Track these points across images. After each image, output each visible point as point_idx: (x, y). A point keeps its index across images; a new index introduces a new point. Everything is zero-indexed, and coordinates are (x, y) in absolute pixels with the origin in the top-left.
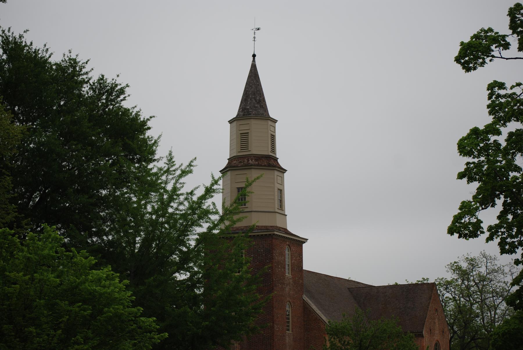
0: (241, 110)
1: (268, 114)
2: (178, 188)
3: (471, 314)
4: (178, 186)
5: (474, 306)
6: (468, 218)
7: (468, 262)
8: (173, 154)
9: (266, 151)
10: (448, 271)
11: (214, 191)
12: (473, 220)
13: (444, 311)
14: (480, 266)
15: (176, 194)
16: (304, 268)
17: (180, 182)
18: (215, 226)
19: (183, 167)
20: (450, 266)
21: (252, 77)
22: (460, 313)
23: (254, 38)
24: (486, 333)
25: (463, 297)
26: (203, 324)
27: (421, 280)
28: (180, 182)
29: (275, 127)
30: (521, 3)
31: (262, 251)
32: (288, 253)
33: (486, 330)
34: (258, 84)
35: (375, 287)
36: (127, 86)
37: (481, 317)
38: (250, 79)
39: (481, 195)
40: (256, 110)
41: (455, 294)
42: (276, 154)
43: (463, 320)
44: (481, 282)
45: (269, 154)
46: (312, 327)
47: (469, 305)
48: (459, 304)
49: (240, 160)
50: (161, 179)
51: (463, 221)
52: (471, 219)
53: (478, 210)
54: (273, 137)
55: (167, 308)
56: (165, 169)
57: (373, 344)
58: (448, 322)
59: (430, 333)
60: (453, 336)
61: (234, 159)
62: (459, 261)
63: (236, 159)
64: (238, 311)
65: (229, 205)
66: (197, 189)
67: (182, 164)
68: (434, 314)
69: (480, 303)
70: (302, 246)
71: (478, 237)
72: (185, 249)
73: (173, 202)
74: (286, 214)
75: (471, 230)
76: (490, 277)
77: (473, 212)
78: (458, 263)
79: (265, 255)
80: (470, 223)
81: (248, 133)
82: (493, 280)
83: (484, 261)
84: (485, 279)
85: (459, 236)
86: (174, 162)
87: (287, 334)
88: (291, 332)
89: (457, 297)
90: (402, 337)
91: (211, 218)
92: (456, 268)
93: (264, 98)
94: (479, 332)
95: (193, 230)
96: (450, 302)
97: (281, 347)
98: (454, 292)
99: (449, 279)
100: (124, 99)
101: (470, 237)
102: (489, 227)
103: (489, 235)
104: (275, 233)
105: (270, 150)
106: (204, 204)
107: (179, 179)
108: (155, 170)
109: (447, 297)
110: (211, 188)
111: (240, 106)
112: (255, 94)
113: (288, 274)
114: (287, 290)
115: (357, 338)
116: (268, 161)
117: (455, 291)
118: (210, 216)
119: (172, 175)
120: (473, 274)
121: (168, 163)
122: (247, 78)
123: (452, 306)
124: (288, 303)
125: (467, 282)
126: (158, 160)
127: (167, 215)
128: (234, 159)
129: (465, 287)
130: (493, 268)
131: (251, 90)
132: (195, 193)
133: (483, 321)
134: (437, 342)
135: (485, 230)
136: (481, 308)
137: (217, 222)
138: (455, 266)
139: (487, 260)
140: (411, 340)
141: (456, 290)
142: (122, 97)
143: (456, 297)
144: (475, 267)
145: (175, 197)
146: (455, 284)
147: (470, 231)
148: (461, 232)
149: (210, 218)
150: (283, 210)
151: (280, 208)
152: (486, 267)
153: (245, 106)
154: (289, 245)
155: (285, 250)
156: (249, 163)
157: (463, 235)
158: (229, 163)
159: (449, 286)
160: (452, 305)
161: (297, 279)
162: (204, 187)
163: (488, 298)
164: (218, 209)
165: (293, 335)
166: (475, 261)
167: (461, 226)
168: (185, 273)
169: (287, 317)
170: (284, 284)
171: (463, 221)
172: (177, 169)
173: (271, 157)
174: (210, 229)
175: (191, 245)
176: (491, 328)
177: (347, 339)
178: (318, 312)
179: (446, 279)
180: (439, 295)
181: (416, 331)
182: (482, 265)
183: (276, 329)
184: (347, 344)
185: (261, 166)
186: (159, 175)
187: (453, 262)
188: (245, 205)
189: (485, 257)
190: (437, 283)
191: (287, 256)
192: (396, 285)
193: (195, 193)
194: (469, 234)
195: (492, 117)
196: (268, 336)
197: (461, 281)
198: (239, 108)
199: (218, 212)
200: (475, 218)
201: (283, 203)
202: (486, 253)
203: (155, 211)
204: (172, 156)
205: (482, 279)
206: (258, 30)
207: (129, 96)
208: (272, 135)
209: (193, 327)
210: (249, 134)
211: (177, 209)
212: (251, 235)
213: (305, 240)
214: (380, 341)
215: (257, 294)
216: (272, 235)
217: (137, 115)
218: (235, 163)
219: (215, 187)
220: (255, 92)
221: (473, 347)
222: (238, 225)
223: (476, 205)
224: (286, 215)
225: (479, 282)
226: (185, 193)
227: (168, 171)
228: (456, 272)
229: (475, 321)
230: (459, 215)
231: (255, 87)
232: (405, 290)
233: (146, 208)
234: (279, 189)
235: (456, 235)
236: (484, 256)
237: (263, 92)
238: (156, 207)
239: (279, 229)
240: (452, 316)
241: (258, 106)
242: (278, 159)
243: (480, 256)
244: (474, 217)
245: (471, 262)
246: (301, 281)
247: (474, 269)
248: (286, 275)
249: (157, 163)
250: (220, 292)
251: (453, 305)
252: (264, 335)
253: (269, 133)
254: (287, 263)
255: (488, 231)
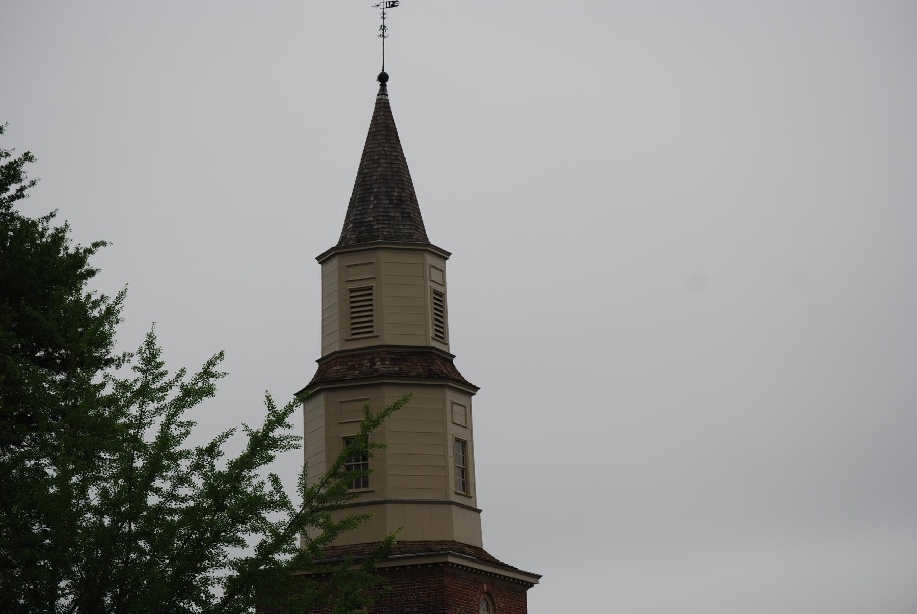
0: (351, 226)
1: (426, 235)
4: (175, 431)
8: (158, 344)
9: (424, 339)
11: (275, 444)
17: (179, 420)
18: (280, 540)
19: (187, 380)
21: (379, 137)
23: (383, 28)
28: (179, 420)
29: (443, 272)
34: (394, 154)
36: (28, 157)
38: (373, 142)
40: (391, 226)
42: (447, 344)
45: (429, 345)
49: (350, 363)
50: (126, 415)
54: (440, 299)
56: (137, 386)
61: (333, 360)
63: (339, 360)
65: (318, 483)
66: (225, 439)
67: (182, 370)
70: (526, 592)
74: (479, 507)
81: (371, 288)
86: (161, 364)
93: (412, 194)
100: (20, 194)
104: (451, 559)
105: (431, 333)
106: (249, 480)
107: (175, 413)
108: (108, 391)
110: (266, 435)
111: (348, 216)
112: (389, 182)
116: (426, 364)
118: (265, 514)
119: (156, 401)
121: (145, 368)
122: (365, 140)
126: (118, 362)
128: (335, 361)
131: (377, 171)
132: (220, 449)
137: (286, 530)
142: (13, 189)
145: (165, 463)
150: (471, 497)
153: (361, 214)
154: (488, 593)
156: (376, 371)
158: (319, 371)
162: (247, 432)
172: (169, 385)
173: (435, 354)
174: (265, 551)
175: (213, 596)
185: (408, 376)
186: (122, 403)
188: (366, 484)
193: (220, 449)
198: (346, 221)
199: (288, 502)
201: (471, 476)
203: (109, 505)
204: (155, 347)
206: (393, 6)
207: (33, 183)
208: (435, 292)
210: (374, 291)
211: (171, 496)
212: (383, 569)
213: (532, 579)
216: (441, 565)
217: (58, 238)
218: (338, 371)
219: (278, 432)
220: (387, 175)
222: (342, 540)
224: (480, 511)
226: (193, 450)
227: (144, 393)
231: (387, 163)
233: (83, 494)
237: (409, 176)
238: (112, 493)
239: (462, 549)
241: (398, 214)
242: (455, 356)
249: (116, 371)
253: (429, 288)
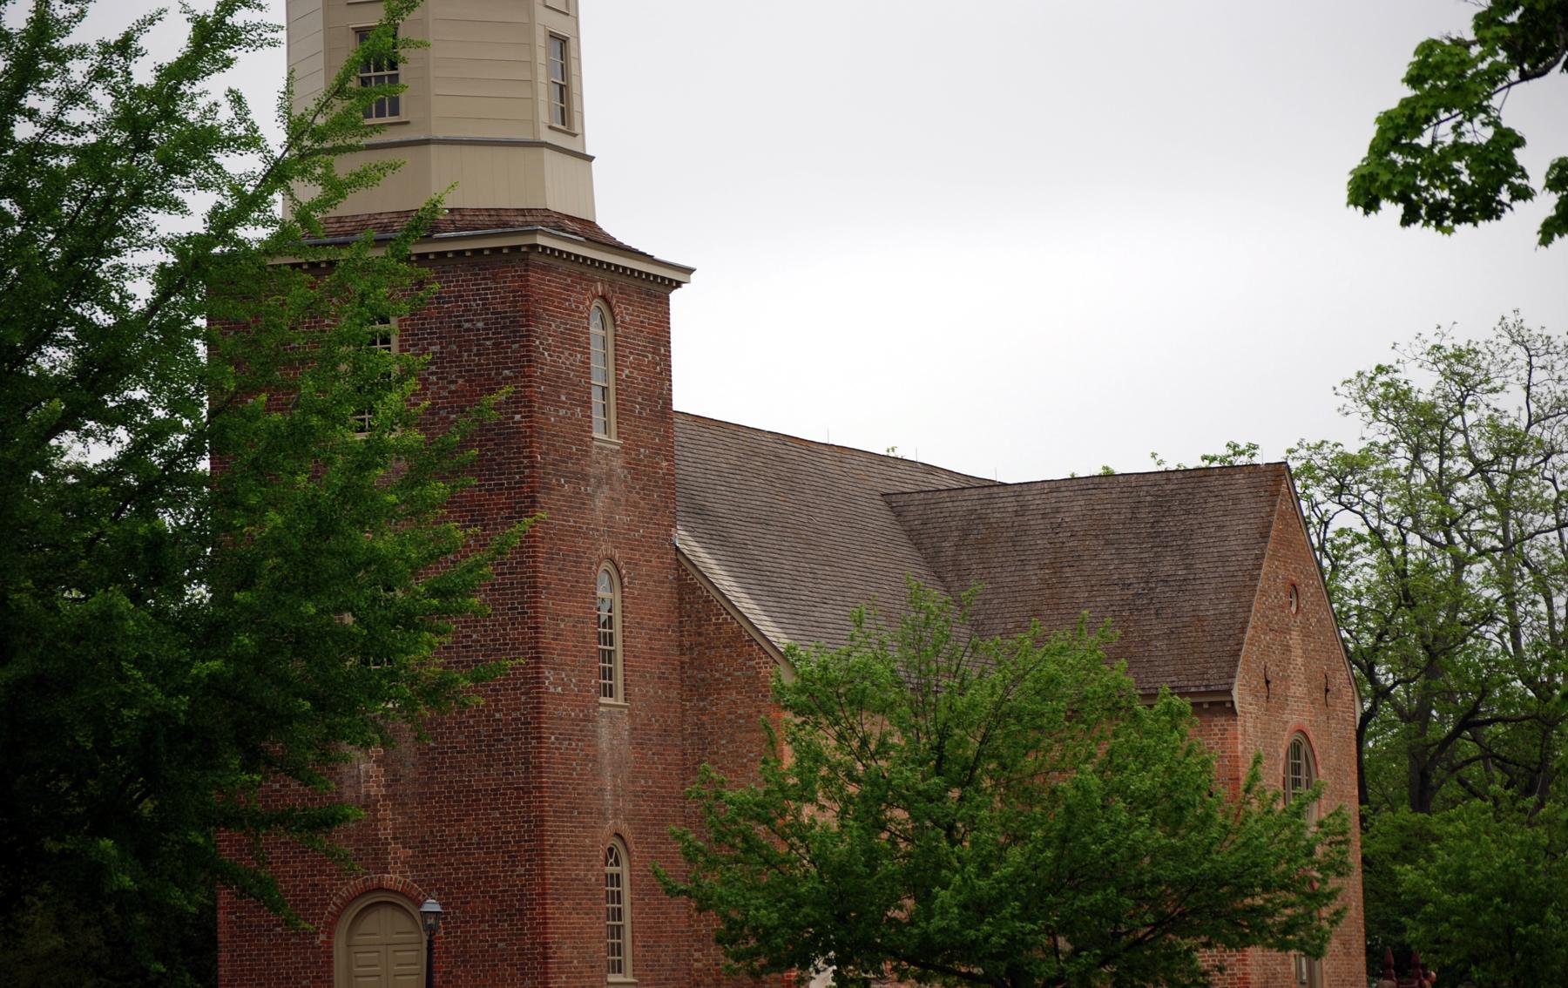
2: (58, 20)
3: (1455, 608)
5: (1471, 572)
6: (1452, 122)
7: (1442, 366)
10: (1346, 409)
12: (1478, 133)
13: (1330, 594)
14: (1498, 383)
15: (50, 49)
16: (679, 404)
18: (248, 204)
20: (1354, 389)
22: (1403, 602)
24: (1530, 693)
25: (1415, 528)
26: (194, 671)
27: (1222, 451)
30: (1424, 39)
31: (480, 325)
32: (601, 332)
33: (1529, 681)
35: (1009, 488)
37: (1506, 619)
39: (1515, 8)
41: (1382, 517)
43: (1422, 636)
44: (1505, 459)
46: (717, 675)
47: (1445, 567)
48: (1402, 560)
51: (1424, 141)
52: (1467, 125)
53: (1502, 80)
55: (16, 597)
57: (997, 748)
58: (1350, 645)
59: (1268, 697)
60: (1374, 708)
62: (1398, 362)
64: (363, 604)
65: (312, 106)
66: (149, 27)
68: (1282, 607)
69: (1498, 555)
70: (668, 299)
71: (1498, 218)
72: (102, 318)
73: (40, 90)
74: (589, 152)
75: (1465, 183)
76: (1546, 436)
77: (1476, 94)
78: (1395, 371)
79: (497, 345)
80: (1458, 150)
82: (1557, 448)
83: (1518, 363)
84: (1522, 442)
85: (1403, 216)
87: (601, 709)
88: (621, 703)
89: (1390, 527)
90: (1136, 715)
91: (224, 167)
92: (1385, 397)
94: (1497, 693)
95: (139, 227)
96: (1357, 554)
97: (574, 769)
98: (1378, 507)
99: (1353, 448)
101: (1457, 221)
102: (1553, 167)
103: (1557, 207)
104: (541, 240)
109: (1341, 532)
110: (220, 22)
113: (603, 433)
114: (600, 503)
115: (922, 722)
117: (1379, 503)
118: (220, 158)
120: (1463, 420)
123: (1366, 569)
124: (606, 565)
125: (1437, 461)
127: (10, 152)
129: (1425, 485)
130: (1559, 394)
133: (1516, 645)
134: (1300, 737)
135: (1537, 181)
136: (1506, 583)
138: (1382, 385)
139: (1530, 356)
140: (1175, 727)
141: (1384, 498)
143: (1385, 531)
144: (1473, 388)
145: (44, 65)
146: (1381, 468)
147: (1462, 192)
148: (1414, 196)
149: (218, 168)
150: (575, 135)
151: (560, 126)
152: (1528, 388)
154: (603, 297)
155: (588, 319)
157: (1423, 212)
159: (1350, 477)
160: (1366, 565)
161: (645, 456)
163: (1538, 532)
164: (257, 124)
165: (630, 715)
166: (1475, 363)
167: (1416, 167)
168: (107, 431)
169: (601, 630)
170: (585, 478)
171: (1424, 141)
174: (222, 222)
175: (132, 298)
176: (1551, 674)
177: (873, 726)
178: (746, 605)
179: (1336, 445)
180: (1307, 522)
181: (1203, 689)
182: (1509, 379)
183: (552, 690)
184: (877, 752)
187: (1369, 369)
188: (395, 111)
189: (1523, 344)
190: (1295, 465)
191: (596, 349)
192: (1108, 475)
194: (1453, 205)
195: (1385, 204)
196: (513, 720)
197: (1409, 455)
199: (260, 138)
200: (1484, 124)
201: (575, 98)
202: (1524, 324)
205: (1511, 443)
209: (149, 686)
211: (56, 124)
214: (1032, 734)
215: (452, 525)
216: (523, 249)
221: (1468, 762)
222: (354, 205)
223: (1490, 60)
225: (1491, 457)
228: (1383, 412)
229: (1477, 637)
230: (1407, 111)
232: (1149, 498)
234: (553, 36)
235: (1391, 211)
236: (1519, 339)
239: (560, 223)
240: (1369, 619)
243: (1500, 340)
244: (1482, 116)
245: (1459, 368)
246: (665, 464)
247: (1469, 398)
248: (593, 438)
250: (274, 518)
251: (1373, 567)
252: (497, 715)
254: (597, 380)
255: (1552, 185)
